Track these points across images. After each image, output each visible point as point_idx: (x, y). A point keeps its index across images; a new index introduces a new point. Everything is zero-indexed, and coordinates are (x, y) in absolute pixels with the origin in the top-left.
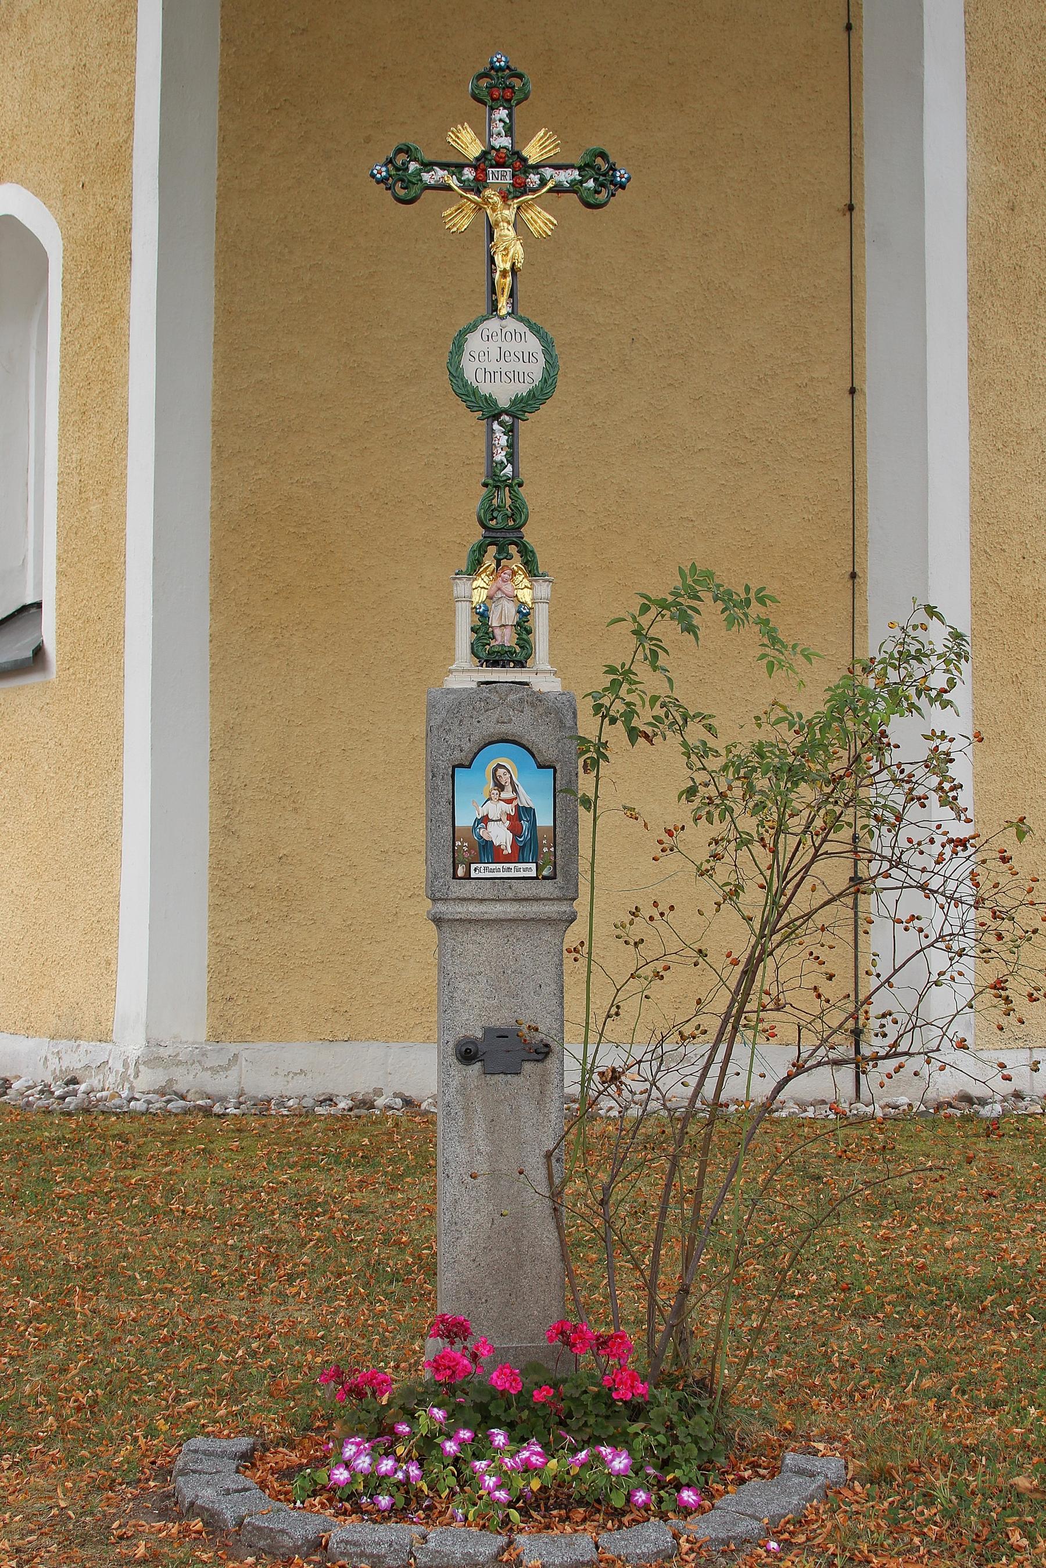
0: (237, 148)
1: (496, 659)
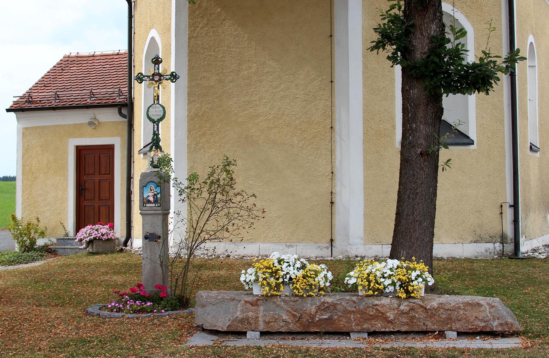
1: (155, 167)
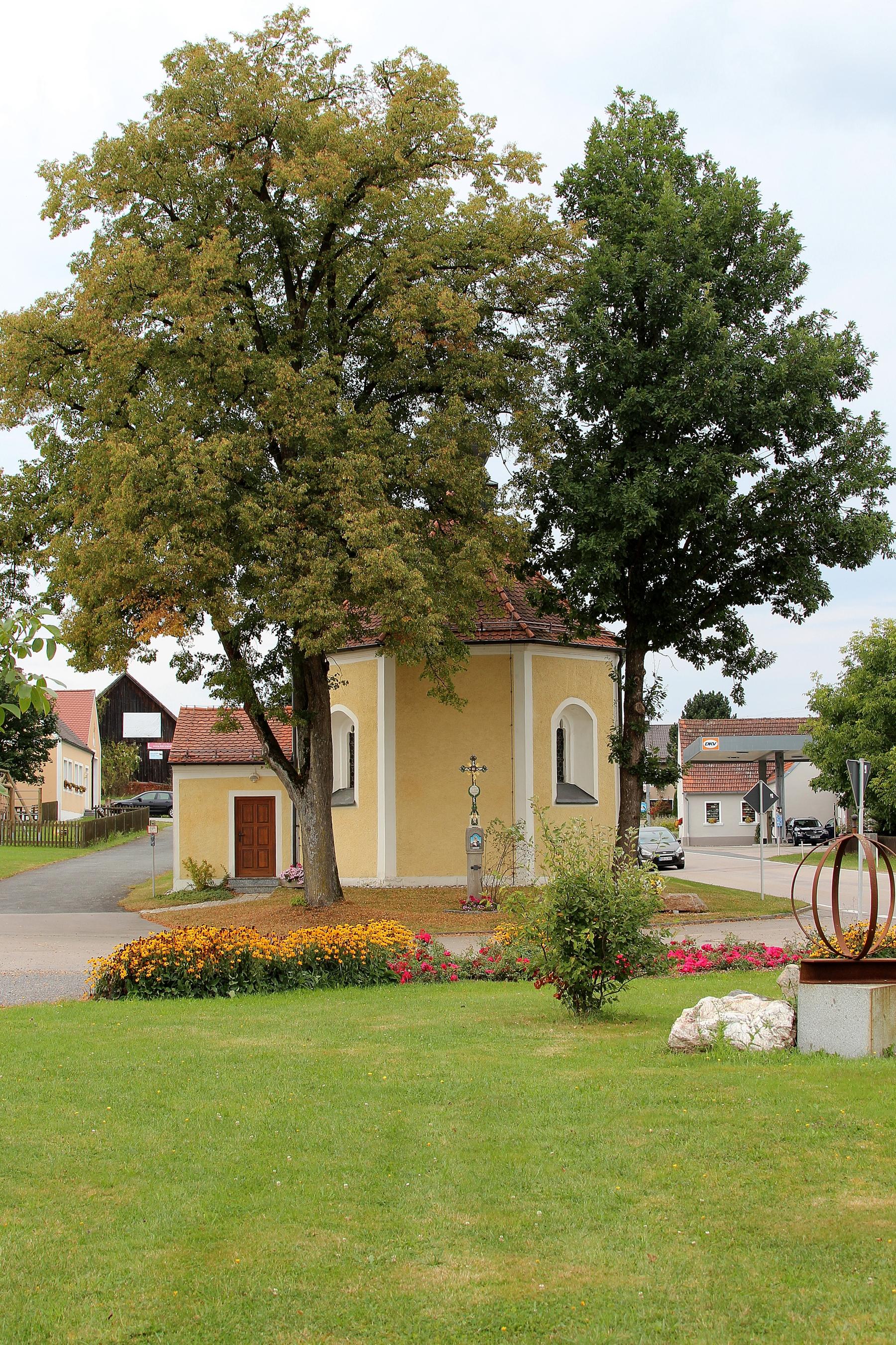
0: (399, 711)
